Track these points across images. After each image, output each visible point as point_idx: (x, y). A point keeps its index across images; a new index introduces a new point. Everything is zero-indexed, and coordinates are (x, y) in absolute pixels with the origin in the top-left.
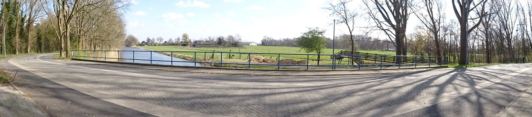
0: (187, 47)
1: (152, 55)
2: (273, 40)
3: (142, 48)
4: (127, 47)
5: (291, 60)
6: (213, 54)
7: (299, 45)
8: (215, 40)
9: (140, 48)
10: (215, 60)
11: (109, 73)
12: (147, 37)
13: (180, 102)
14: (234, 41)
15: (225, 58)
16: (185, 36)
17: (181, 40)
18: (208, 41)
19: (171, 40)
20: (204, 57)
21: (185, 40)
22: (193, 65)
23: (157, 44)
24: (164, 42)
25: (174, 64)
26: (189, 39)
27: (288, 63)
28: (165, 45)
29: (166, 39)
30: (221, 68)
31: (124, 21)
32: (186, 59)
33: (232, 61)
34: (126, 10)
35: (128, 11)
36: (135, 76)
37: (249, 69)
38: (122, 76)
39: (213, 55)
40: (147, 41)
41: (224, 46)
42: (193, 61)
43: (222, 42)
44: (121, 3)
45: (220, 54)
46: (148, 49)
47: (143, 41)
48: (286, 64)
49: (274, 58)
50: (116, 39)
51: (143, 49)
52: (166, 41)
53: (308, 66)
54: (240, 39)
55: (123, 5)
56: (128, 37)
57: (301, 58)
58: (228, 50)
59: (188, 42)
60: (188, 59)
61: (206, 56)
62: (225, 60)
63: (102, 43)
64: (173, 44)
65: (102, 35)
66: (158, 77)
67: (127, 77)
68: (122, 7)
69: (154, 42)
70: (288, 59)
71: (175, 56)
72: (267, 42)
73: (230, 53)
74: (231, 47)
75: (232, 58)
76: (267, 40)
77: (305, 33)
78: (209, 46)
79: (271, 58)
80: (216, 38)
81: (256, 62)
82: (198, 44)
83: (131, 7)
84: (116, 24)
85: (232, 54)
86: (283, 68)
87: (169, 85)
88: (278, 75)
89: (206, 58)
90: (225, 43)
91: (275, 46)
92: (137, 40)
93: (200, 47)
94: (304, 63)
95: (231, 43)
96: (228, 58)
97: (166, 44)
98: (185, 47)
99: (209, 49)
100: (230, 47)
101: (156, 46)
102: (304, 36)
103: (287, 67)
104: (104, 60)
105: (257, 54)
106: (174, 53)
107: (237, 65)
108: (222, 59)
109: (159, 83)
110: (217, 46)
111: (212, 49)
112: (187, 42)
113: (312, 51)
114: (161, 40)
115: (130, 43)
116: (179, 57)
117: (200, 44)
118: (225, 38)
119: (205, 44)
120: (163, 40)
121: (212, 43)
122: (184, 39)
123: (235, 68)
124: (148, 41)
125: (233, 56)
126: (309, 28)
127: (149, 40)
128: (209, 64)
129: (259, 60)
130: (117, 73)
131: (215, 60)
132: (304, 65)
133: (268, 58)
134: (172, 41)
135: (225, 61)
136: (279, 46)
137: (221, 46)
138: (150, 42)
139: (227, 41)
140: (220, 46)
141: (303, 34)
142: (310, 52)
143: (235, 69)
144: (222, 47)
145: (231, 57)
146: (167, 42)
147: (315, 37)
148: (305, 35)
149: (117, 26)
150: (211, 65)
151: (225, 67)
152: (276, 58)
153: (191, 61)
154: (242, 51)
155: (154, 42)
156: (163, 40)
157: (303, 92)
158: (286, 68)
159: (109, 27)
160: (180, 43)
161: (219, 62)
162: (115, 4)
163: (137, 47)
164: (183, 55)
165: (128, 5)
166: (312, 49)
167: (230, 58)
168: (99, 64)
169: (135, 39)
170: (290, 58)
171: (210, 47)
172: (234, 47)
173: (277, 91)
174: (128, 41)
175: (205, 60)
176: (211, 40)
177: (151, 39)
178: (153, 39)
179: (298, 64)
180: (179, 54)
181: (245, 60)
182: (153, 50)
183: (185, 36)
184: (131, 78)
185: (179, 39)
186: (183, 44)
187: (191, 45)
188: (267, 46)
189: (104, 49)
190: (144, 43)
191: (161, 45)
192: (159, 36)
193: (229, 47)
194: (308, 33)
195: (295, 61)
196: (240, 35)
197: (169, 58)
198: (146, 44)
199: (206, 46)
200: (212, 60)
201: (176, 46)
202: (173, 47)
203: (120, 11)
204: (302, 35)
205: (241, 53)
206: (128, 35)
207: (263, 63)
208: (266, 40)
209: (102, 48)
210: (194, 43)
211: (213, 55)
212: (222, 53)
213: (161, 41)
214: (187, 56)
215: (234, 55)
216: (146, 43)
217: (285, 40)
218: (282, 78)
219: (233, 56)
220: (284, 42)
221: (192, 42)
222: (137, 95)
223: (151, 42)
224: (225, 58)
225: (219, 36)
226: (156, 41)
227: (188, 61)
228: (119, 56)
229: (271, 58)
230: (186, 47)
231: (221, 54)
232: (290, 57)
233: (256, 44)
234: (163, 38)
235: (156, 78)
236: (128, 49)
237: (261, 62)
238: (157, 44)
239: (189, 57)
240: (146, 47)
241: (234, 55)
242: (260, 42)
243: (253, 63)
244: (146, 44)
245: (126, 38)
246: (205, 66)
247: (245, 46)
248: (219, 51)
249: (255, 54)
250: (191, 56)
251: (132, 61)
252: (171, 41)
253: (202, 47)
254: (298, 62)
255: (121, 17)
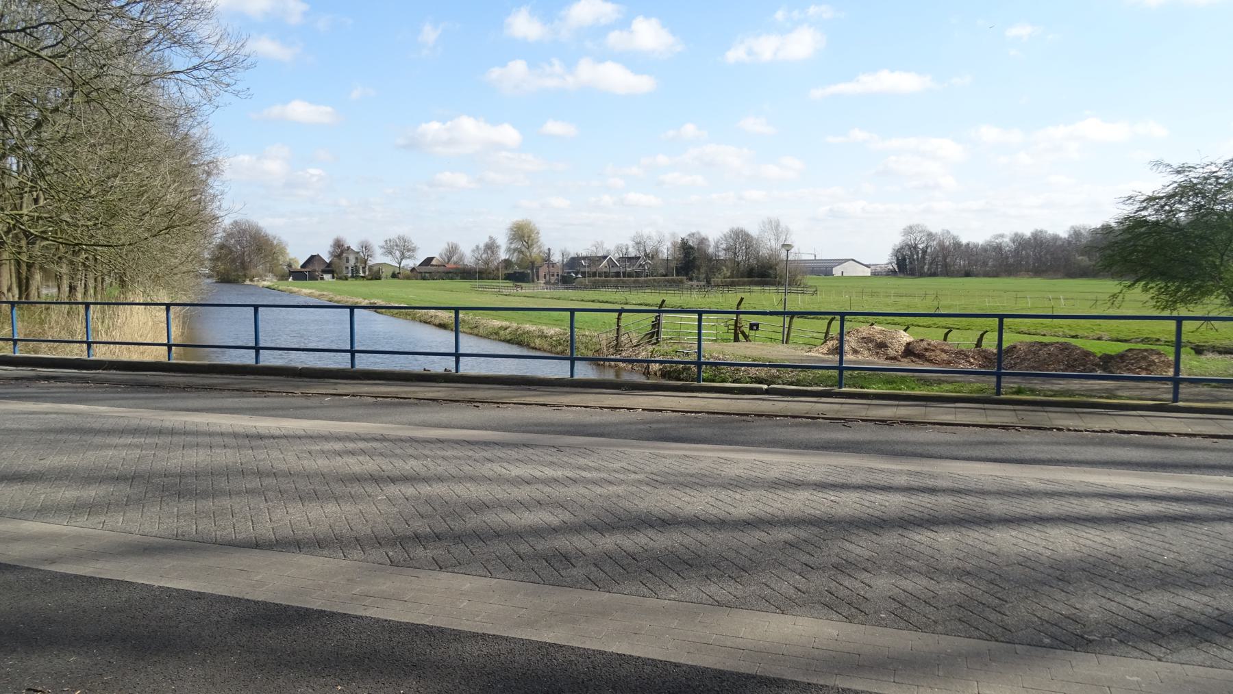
0: (531, 285)
1: (356, 327)
2: (957, 245)
3: (308, 291)
4: (226, 286)
5: (1064, 347)
6: (658, 319)
7: (1111, 266)
8: (665, 251)
9: (296, 289)
10: (664, 348)
11: (109, 424)
12: (335, 236)
13: (502, 548)
14: (757, 258)
15: (715, 341)
16: (522, 234)
17: (503, 255)
18: (630, 258)
19: (452, 250)
20: (613, 335)
21: (520, 252)
22: (557, 370)
23: (386, 272)
24: (418, 263)
25: (469, 367)
26: (540, 247)
27: (1044, 363)
28: (424, 279)
29: (430, 247)
30: (696, 384)
31: (206, 144)
32: (528, 346)
33: (748, 352)
34: (211, 89)
35: (226, 97)
36: (263, 432)
37: (837, 390)
38: (186, 433)
39: (656, 325)
40: (331, 254)
41: (708, 282)
42: (563, 352)
43: (698, 263)
44: (187, 51)
45: (693, 320)
46: (338, 298)
47: (312, 257)
48: (1034, 368)
49: (963, 339)
50: (157, 242)
51: (310, 295)
52: (432, 259)
53: (1176, 381)
54: (787, 247)
55: (196, 61)
56: (230, 235)
57: (1121, 336)
58: (728, 299)
59: (537, 264)
60: (538, 341)
61: (622, 331)
62: (714, 350)
63: (72, 263)
64: (466, 274)
65: (66, 217)
66: (385, 432)
67: (219, 440)
68: (195, 73)
69: (371, 262)
70: (1046, 345)
71: (475, 332)
72: (923, 257)
73: (738, 313)
74: (744, 284)
75: (746, 337)
76: (921, 246)
77: (1150, 199)
78: (635, 282)
79: (945, 339)
80: (669, 244)
81: (866, 358)
82: (584, 274)
83: (242, 78)
84: (156, 161)
85: (746, 320)
86: (1019, 392)
87: (441, 468)
88: (968, 425)
89: (624, 339)
90: (713, 265)
91: (968, 274)
92: (282, 251)
93: (596, 286)
94: (1143, 364)
95: (742, 268)
96: (728, 340)
97: (428, 271)
98: (523, 285)
99: (637, 297)
100: (738, 284)
101: (379, 278)
102: (1143, 213)
103: (1037, 384)
104: (85, 357)
105: (871, 319)
106: (471, 313)
107: (774, 371)
108: (704, 344)
109: (393, 460)
110: (674, 281)
111: (652, 298)
112: (533, 263)
113: (1197, 293)
114: (405, 249)
115: (243, 263)
116: (494, 335)
117: (594, 274)
118: (712, 244)
119: (617, 274)
120: (413, 250)
121: (655, 267)
122: (515, 250)
123: (765, 387)
124: (339, 256)
125: (754, 327)
126: (1175, 166)
127: (340, 250)
128: (637, 366)
129: (882, 345)
130: (154, 424)
131: (664, 348)
132: (1143, 375)
133: (934, 336)
134: (461, 258)
135: (715, 354)
136: (987, 275)
137: (695, 283)
138: (347, 261)
139: (722, 255)
140: (691, 279)
141: (1136, 207)
142: (1184, 301)
143: (767, 392)
144: (700, 288)
145: (743, 333)
146: (434, 262)
147: (1220, 215)
148: (1150, 211)
149: (163, 169)
150: (647, 373)
151: (713, 381)
152: (973, 337)
153: (551, 352)
154: (798, 302)
155: (371, 262)
156: (413, 250)
157: (1162, 526)
158: (1033, 391)
159: (115, 176)
160: (497, 269)
161: (687, 359)
162: (148, 48)
163: (283, 285)
164: (515, 325)
165: (229, 64)
166: (1199, 287)
167: (741, 336)
168: (47, 378)
169: (272, 244)
170: (1054, 339)
171: (639, 286)
172: (757, 284)
173: (997, 506)
174: (231, 252)
175: (617, 347)
176: (647, 255)
177: (355, 248)
178: (366, 247)
179: (1104, 370)
180: (495, 322)
181: (811, 346)
182: (365, 303)
183: (522, 234)
184: (240, 441)
185: (491, 247)
186: (511, 271)
187: (553, 280)
188: (922, 275)
189: (85, 294)
190: (318, 268)
191: (408, 278)
192: (394, 232)
193: (733, 284)
194: (1170, 197)
195: (1087, 354)
196: (782, 225)
197: (444, 340)
198: (329, 269)
199: (624, 282)
200: (650, 348)
201: (478, 283)
202: (466, 284)
203: (171, 92)
204: (1129, 210)
205: (793, 314)
206: (227, 222)
207: (906, 364)
208: (915, 247)
209: (72, 288)
210: (564, 266)
211: (656, 325)
212: (700, 313)
213: (403, 257)
214: (533, 328)
215: (757, 325)
216: (329, 265)
217: (1023, 244)
218: (1021, 440)
219: (754, 327)
220: (1017, 252)
221: (554, 265)
222: (269, 526)
223: (352, 262)
224: (715, 341)
225: (684, 235)
226: (379, 258)
227: (549, 355)
228: (173, 329)
229: (945, 339)
230: (527, 289)
231: (700, 320)
232: (1053, 334)
233: (868, 266)
234: (416, 241)
235: (376, 440)
236: (230, 294)
237: (894, 358)
238: (386, 272)
239: (543, 336)
240: (328, 287)
241: (757, 325)
242: (883, 257)
243: (855, 362)
244: (329, 269)
245: (218, 239)
246: (617, 375)
247: (811, 280)
248: (694, 306)
249: (861, 318)
250: (552, 331)
251: (248, 358)
252: (454, 259)
253: (604, 285)
254: (1107, 361)
255: (185, 123)
